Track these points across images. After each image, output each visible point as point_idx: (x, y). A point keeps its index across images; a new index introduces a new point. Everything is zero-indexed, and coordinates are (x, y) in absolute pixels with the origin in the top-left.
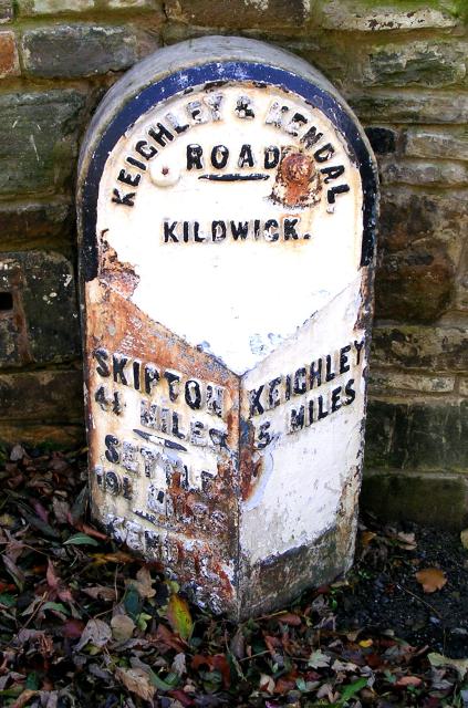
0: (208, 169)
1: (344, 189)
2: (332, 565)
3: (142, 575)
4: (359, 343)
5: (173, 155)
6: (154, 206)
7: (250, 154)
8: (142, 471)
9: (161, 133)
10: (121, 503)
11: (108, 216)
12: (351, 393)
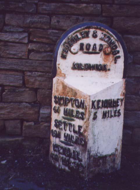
0: (85, 50)
1: (119, 57)
2: (114, 166)
3: (5, 28)
4: (122, 99)
5: (75, 47)
6: (72, 59)
7: (96, 46)
8: (63, 128)
9: (74, 39)
10: (58, 139)
11: (60, 61)
12: (119, 112)
